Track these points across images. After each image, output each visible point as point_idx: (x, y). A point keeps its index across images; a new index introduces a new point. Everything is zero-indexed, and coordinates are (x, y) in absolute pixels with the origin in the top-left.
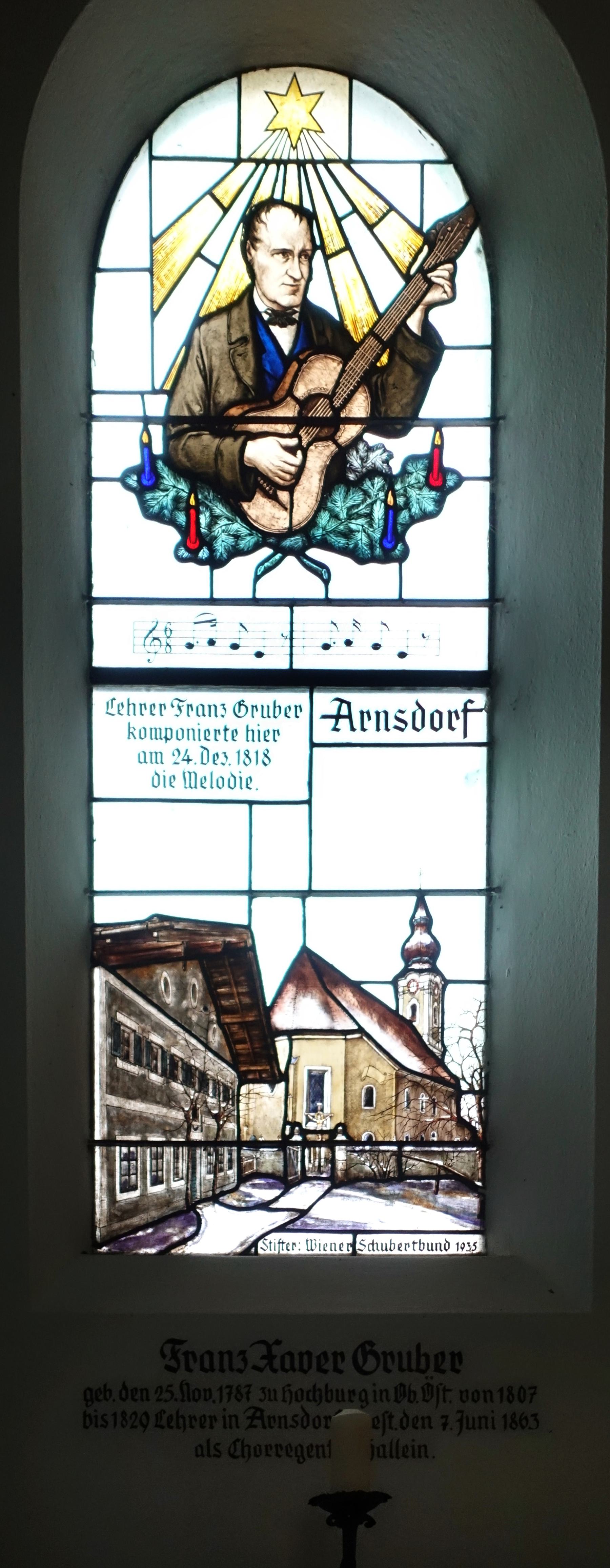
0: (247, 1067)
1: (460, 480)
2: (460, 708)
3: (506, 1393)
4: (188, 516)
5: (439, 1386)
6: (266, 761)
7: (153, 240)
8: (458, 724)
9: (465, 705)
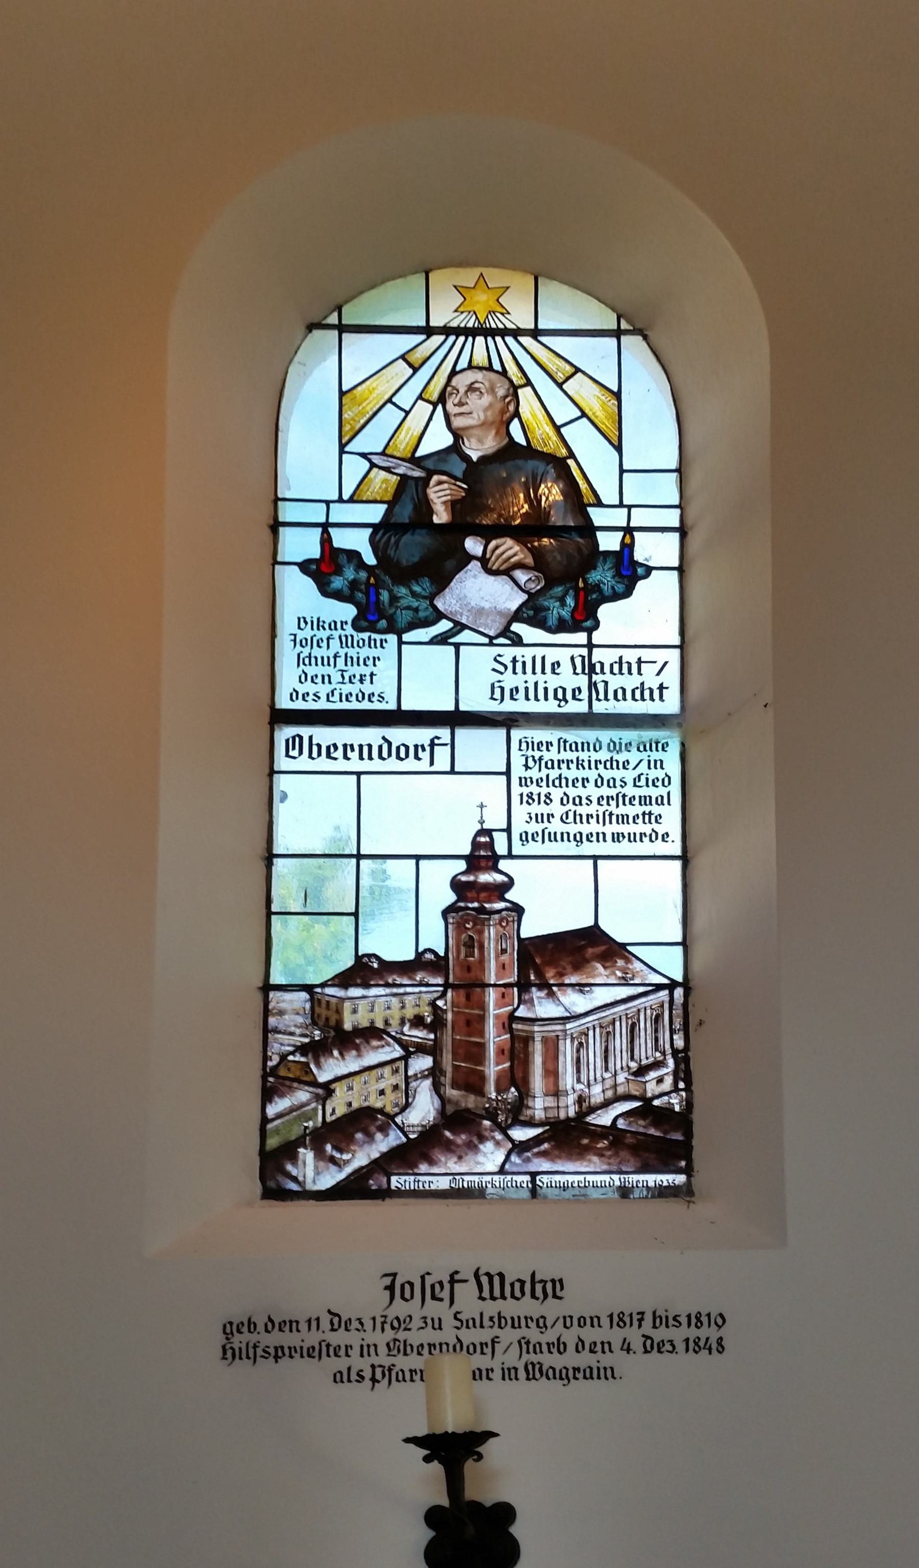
0: (425, 1032)
1: (649, 570)
2: (427, 743)
3: (616, 1319)
4: (367, 594)
5: (522, 1340)
6: (548, 801)
7: (342, 394)
8: (425, 755)
9: (432, 741)
